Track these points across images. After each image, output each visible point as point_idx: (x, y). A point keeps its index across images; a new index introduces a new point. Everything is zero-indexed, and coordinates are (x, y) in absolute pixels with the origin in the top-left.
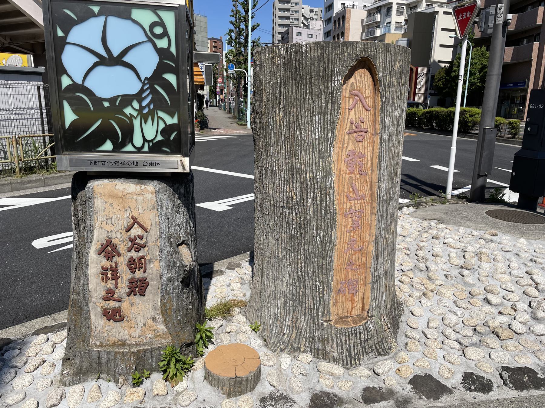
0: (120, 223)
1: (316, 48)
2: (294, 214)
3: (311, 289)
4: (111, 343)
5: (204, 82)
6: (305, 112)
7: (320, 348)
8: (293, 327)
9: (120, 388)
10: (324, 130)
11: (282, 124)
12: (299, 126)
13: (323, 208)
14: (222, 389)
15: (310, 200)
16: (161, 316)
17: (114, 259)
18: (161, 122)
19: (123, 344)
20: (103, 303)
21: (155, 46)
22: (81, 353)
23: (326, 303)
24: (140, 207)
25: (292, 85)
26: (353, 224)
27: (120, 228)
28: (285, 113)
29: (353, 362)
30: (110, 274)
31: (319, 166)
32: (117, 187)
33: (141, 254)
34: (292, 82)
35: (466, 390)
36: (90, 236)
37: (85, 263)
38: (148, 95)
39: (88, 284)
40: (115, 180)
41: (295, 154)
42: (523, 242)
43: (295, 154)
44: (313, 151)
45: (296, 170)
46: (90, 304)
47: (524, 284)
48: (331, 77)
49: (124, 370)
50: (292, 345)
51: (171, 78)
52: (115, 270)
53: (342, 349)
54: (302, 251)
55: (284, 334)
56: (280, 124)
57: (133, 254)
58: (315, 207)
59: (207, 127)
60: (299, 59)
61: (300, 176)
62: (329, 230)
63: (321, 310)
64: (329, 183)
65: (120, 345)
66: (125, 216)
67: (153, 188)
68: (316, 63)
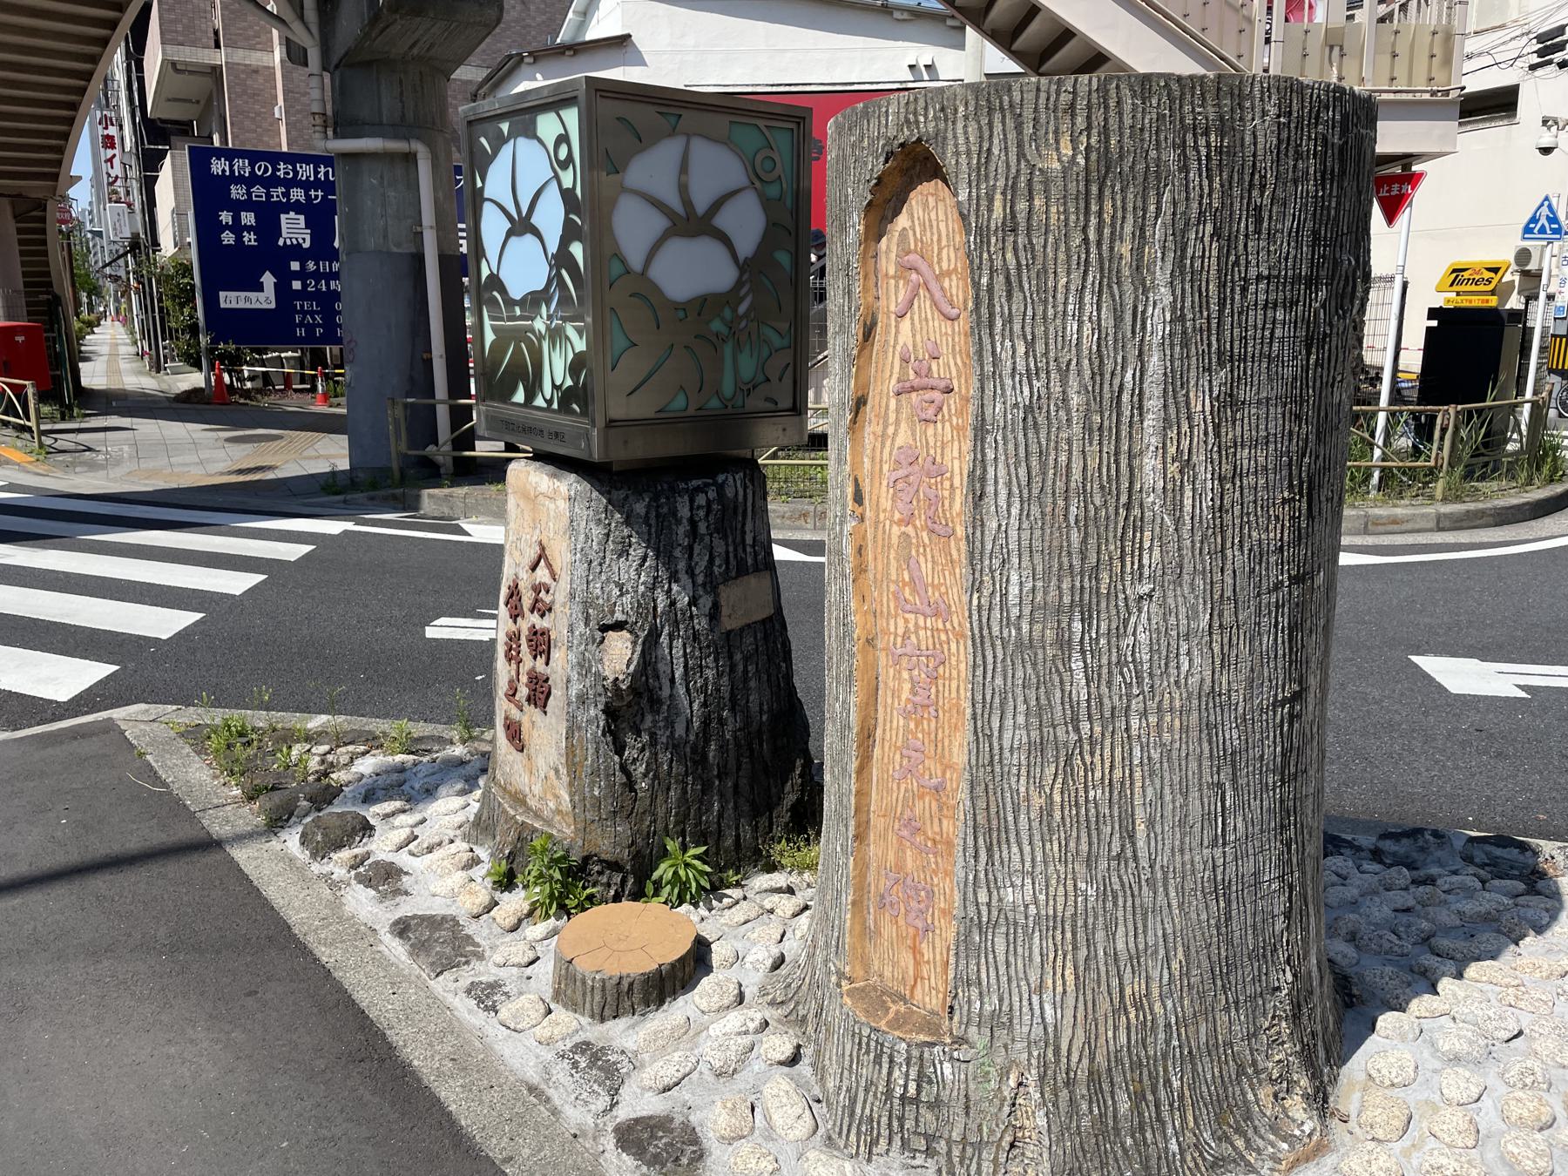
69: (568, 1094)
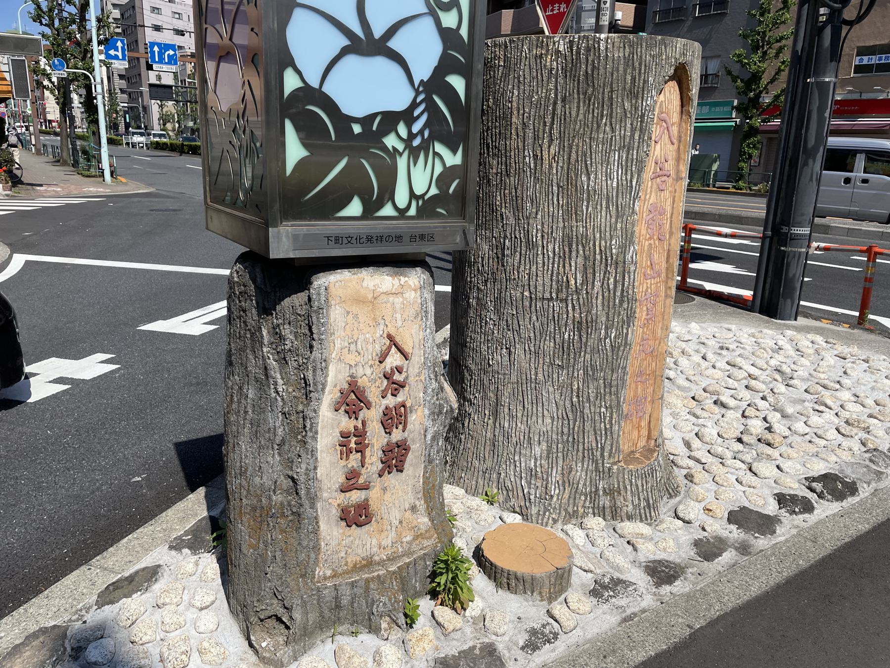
0: (370, 347)
1: (622, 45)
2: (570, 308)
3: (594, 421)
4: (351, 565)
5: (11, 92)
6: (598, 145)
7: (607, 504)
8: (564, 482)
9: (387, 639)
10: (626, 174)
11: (554, 165)
12: (586, 167)
13: (618, 294)
14: (540, 593)
15: (598, 284)
16: (423, 502)
17: (361, 415)
18: (437, 162)
19: (369, 563)
20: (342, 499)
21: (438, 23)
22: (302, 598)
23: (615, 436)
24: (398, 316)
25: (579, 103)
26: (647, 315)
27: (370, 357)
28: (562, 147)
29: (653, 514)
30: (353, 442)
31: (616, 229)
32: (365, 284)
33: (400, 399)
34: (579, 98)
35: (791, 514)
36: (320, 378)
37: (311, 429)
38: (422, 113)
39: (315, 468)
40: (359, 270)
41: (576, 213)
42: (694, 326)
43: (576, 213)
44: (608, 207)
45: (577, 238)
46: (319, 505)
47: (740, 377)
48: (643, 91)
49: (389, 605)
50: (566, 510)
51: (457, 83)
52: (360, 434)
53: (639, 499)
54: (581, 365)
55: (552, 497)
56: (550, 166)
57: (390, 401)
58: (606, 294)
59: (22, 183)
60: (593, 61)
61: (584, 247)
62: (625, 327)
63: (608, 448)
64: (631, 254)
65: (365, 566)
66: (378, 335)
67: (416, 281)
68: (621, 68)
69: (637, 600)
